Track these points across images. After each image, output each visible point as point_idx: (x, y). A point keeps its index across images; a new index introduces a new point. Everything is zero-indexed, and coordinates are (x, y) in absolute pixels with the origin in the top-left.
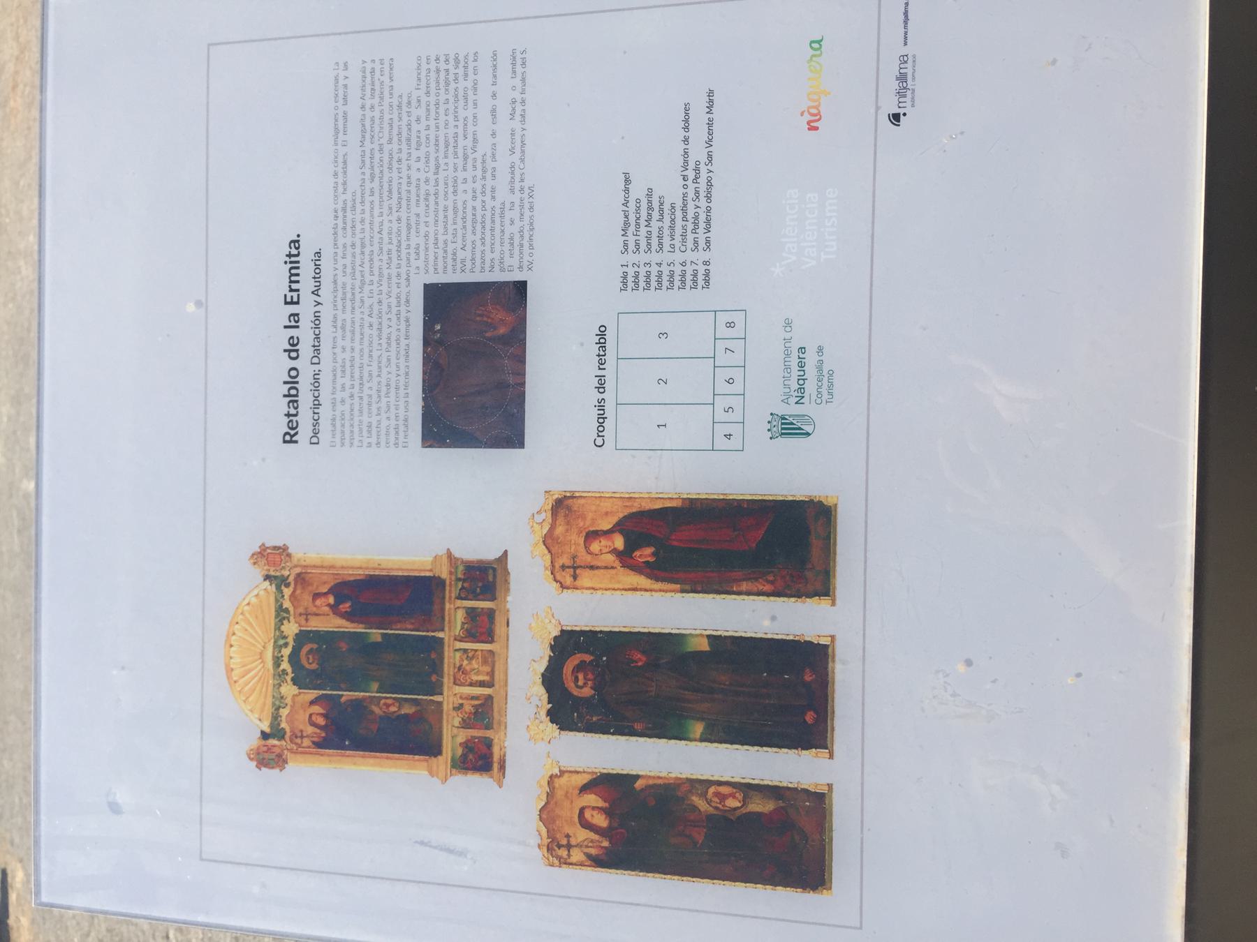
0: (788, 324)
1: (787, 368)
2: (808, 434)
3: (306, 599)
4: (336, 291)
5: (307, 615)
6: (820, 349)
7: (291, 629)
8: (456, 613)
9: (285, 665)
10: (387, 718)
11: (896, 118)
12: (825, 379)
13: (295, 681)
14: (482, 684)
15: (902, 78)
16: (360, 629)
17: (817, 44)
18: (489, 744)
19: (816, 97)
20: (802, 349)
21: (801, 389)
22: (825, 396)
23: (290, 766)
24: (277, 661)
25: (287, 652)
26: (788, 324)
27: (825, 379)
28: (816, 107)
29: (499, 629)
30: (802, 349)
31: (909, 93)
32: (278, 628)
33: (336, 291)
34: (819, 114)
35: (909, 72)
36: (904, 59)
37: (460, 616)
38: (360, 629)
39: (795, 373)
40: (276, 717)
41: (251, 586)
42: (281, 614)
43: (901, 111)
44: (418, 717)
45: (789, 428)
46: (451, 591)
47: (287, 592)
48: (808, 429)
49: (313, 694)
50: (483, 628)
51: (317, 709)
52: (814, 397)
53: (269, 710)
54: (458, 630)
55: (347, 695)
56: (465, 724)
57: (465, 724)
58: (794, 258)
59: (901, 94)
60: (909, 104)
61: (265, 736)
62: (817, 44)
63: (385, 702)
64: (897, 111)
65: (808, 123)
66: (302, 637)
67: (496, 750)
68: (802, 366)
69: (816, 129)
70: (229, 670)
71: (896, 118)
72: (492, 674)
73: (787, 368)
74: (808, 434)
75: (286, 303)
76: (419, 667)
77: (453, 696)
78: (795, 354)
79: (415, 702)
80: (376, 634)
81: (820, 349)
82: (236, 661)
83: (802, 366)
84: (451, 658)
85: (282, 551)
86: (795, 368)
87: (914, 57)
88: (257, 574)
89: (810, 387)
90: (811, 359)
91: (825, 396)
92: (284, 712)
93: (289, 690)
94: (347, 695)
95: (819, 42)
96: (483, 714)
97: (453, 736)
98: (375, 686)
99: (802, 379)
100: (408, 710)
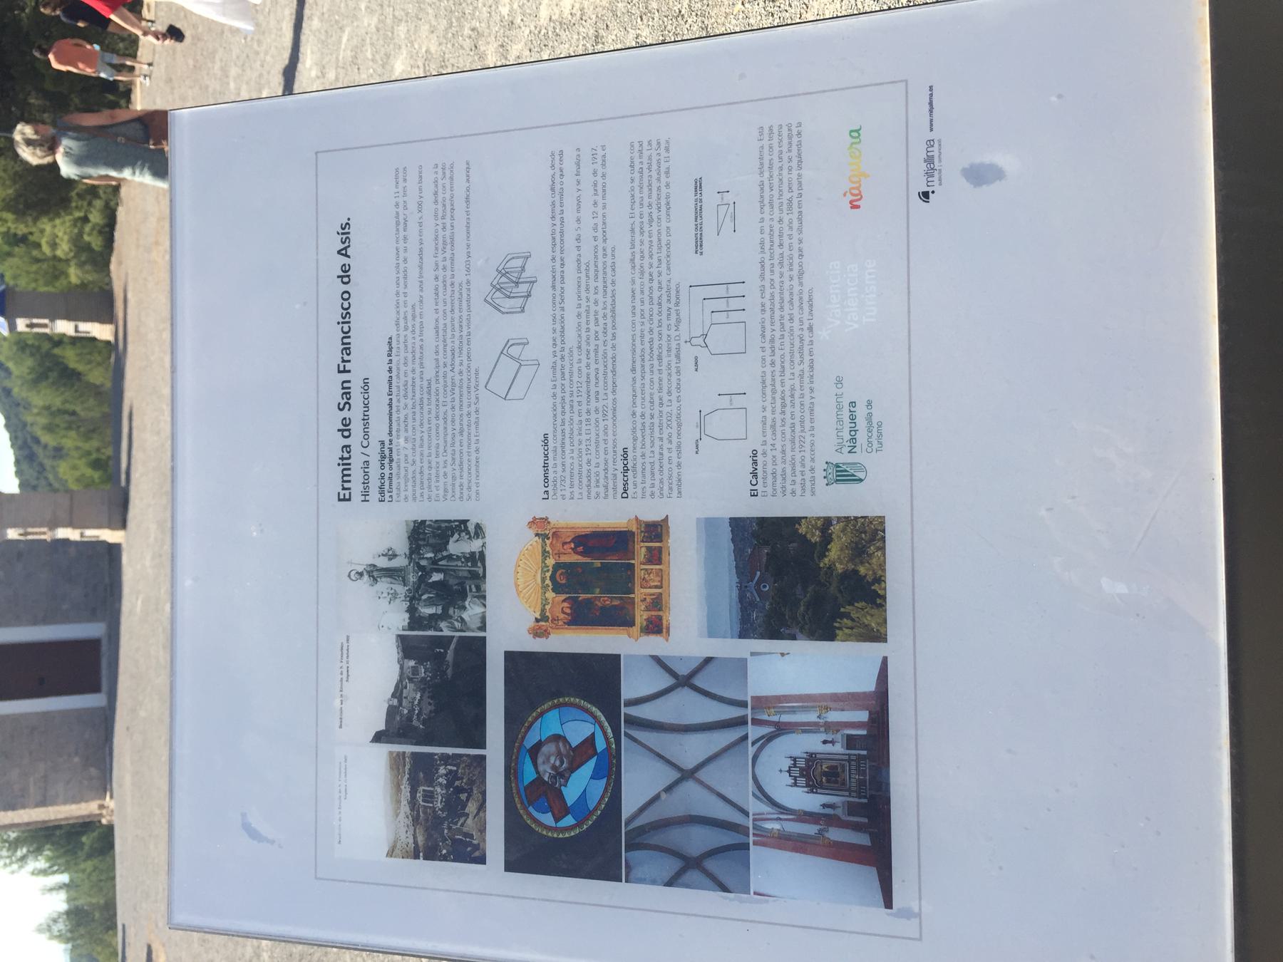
0: (839, 381)
1: (840, 421)
2: (861, 480)
3: (559, 545)
4: (421, 358)
5: (559, 554)
6: (869, 404)
7: (551, 562)
8: (641, 550)
9: (548, 582)
10: (603, 608)
11: (925, 196)
12: (875, 430)
13: (553, 590)
14: (656, 587)
15: (929, 160)
16: (588, 560)
17: (856, 133)
18: (660, 618)
19: (856, 179)
20: (853, 404)
21: (853, 439)
22: (875, 445)
23: (552, 636)
24: (543, 580)
25: (548, 574)
26: (839, 381)
27: (875, 430)
28: (858, 188)
29: (664, 556)
30: (853, 404)
31: (936, 173)
32: (543, 562)
33: (421, 358)
34: (860, 194)
35: (936, 154)
36: (930, 143)
37: (643, 550)
38: (588, 560)
39: (847, 425)
40: (543, 610)
41: (529, 538)
42: (545, 554)
43: (930, 189)
44: (621, 608)
45: (843, 475)
46: (638, 538)
47: (548, 542)
48: (861, 475)
49: (564, 597)
50: (656, 557)
51: (566, 604)
52: (865, 447)
53: (539, 607)
54: (642, 558)
55: (582, 596)
56: (647, 609)
57: (647, 609)
58: (838, 322)
59: (929, 174)
60: (936, 183)
61: (537, 620)
62: (856, 133)
63: (604, 599)
64: (926, 189)
65: (851, 202)
66: (557, 566)
67: (664, 622)
68: (853, 419)
69: (858, 207)
70: (517, 586)
71: (925, 196)
72: (661, 581)
73: (840, 421)
74: (861, 480)
75: (340, 372)
76: (622, 579)
77: (639, 593)
78: (846, 408)
79: (621, 598)
80: (597, 563)
81: (869, 404)
82: (521, 581)
83: (853, 419)
84: (639, 573)
85: (545, 520)
86: (846, 419)
87: (939, 141)
88: (530, 534)
89: (862, 437)
90: (861, 412)
91: (875, 445)
92: (548, 607)
93: (550, 595)
94: (582, 596)
95: (857, 131)
96: (657, 603)
97: (641, 616)
98: (598, 590)
99: (854, 430)
100: (616, 603)
